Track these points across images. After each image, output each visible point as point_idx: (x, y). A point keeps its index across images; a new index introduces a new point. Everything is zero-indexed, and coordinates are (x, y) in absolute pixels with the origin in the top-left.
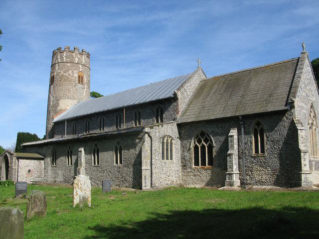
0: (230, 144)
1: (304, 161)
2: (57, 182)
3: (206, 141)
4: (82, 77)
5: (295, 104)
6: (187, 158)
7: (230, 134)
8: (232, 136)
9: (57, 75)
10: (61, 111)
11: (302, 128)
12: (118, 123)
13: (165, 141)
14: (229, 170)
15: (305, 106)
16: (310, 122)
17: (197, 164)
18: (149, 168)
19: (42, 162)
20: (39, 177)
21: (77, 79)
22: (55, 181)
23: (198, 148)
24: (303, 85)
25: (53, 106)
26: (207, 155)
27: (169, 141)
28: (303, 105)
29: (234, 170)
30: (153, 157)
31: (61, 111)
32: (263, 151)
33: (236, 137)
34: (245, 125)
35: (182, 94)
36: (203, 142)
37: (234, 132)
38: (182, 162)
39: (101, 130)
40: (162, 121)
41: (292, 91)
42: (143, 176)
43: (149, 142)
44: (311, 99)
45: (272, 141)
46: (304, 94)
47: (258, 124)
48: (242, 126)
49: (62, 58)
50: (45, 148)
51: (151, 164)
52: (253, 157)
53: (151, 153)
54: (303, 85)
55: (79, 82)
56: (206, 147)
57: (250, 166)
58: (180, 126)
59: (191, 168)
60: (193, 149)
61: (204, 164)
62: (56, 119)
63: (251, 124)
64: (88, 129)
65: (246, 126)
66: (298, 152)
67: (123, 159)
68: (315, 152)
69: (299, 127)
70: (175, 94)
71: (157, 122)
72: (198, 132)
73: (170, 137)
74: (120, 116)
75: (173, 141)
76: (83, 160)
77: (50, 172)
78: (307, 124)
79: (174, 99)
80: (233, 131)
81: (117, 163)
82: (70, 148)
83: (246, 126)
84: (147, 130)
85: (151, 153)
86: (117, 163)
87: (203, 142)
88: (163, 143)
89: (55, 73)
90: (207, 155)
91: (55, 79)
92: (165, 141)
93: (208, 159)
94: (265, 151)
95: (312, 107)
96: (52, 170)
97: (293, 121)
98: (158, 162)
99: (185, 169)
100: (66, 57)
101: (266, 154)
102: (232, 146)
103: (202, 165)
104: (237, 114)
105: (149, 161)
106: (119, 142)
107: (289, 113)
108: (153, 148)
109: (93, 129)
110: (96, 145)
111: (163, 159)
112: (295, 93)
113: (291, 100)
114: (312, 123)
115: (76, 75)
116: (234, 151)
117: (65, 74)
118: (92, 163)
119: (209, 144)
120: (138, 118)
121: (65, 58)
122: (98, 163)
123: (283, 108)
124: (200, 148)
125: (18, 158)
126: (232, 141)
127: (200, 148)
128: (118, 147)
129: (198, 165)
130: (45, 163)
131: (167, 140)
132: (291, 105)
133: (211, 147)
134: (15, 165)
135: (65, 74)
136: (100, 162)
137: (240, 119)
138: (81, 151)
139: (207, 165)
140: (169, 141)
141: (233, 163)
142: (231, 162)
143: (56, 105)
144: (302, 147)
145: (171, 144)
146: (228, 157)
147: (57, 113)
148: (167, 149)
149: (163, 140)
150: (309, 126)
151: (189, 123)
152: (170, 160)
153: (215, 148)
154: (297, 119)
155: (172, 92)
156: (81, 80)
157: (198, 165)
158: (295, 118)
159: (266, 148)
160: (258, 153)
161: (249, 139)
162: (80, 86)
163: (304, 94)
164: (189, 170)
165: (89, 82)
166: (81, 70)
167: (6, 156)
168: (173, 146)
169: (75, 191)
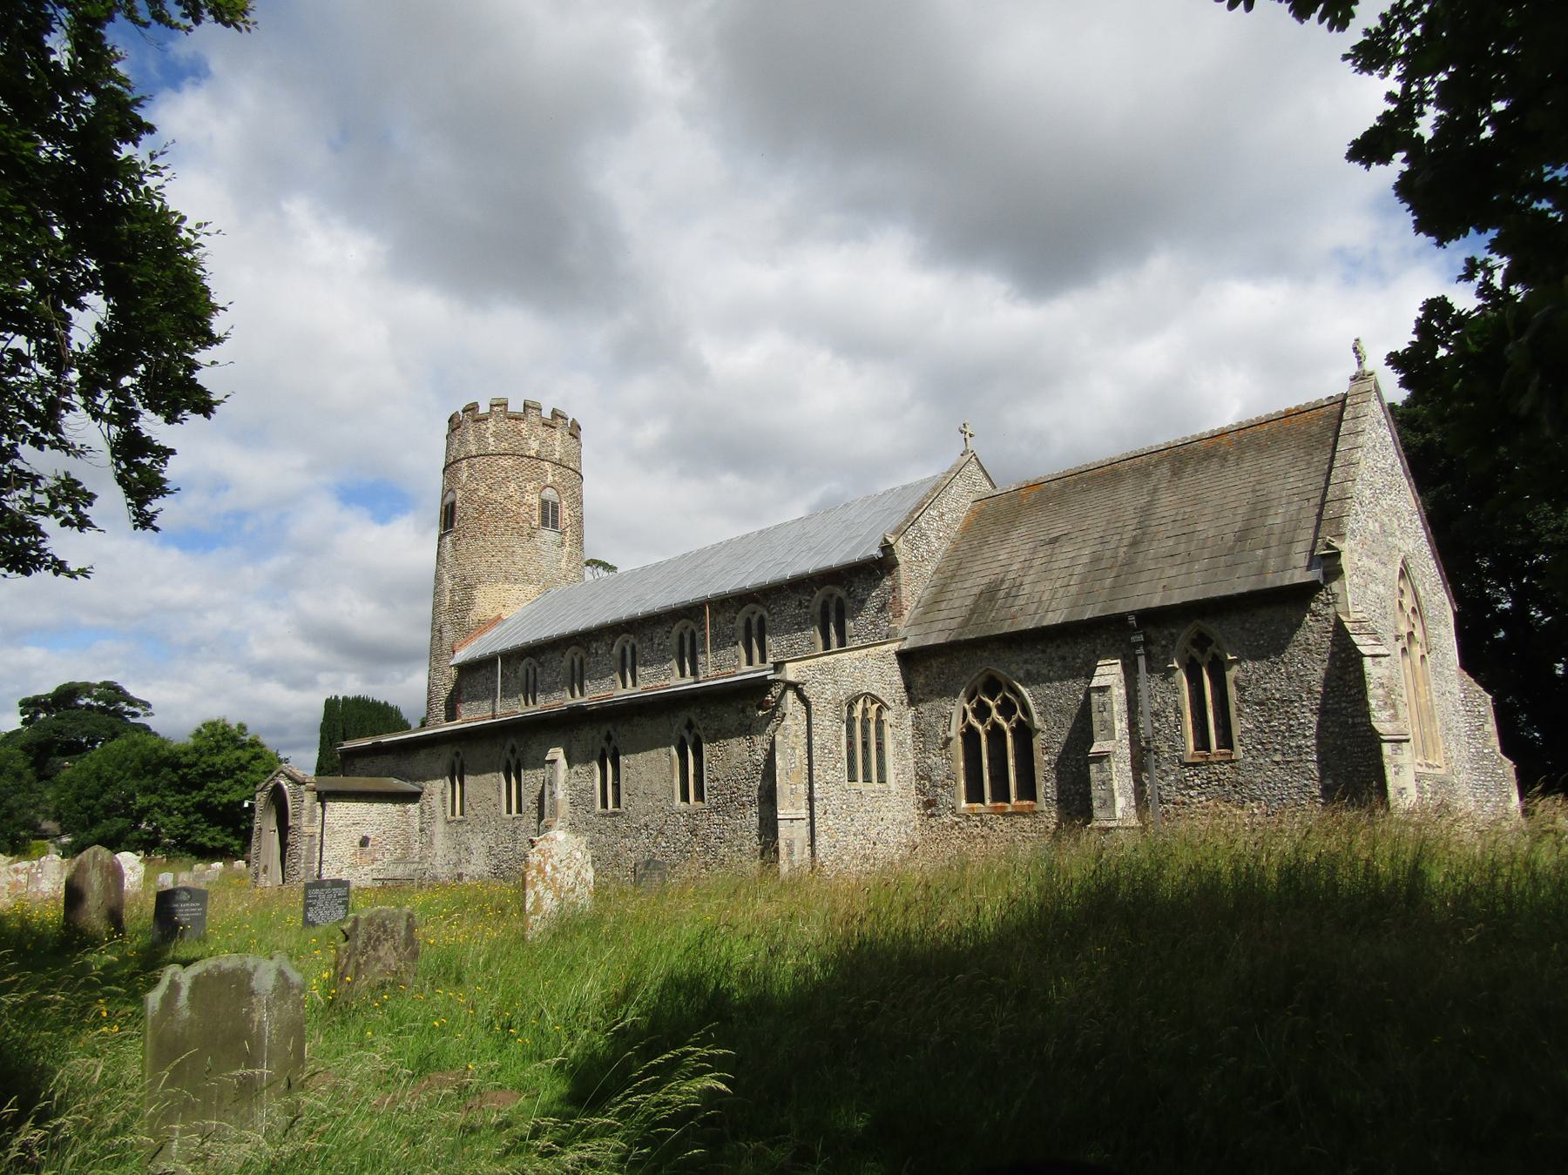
0: (1096, 718)
1: (1397, 773)
2: (466, 879)
3: (1007, 709)
4: (555, 507)
5: (1345, 562)
6: (938, 776)
7: (1095, 683)
8: (1103, 689)
9: (467, 500)
10: (486, 625)
11: (1379, 650)
12: (688, 654)
13: (858, 713)
14: (1097, 813)
15: (1381, 572)
16: (1404, 629)
17: (975, 794)
18: (804, 813)
19: (413, 808)
20: (398, 861)
21: (536, 514)
22: (460, 876)
23: (1004, 734)
24: (1368, 493)
25: (453, 608)
26: (1011, 762)
27: (872, 714)
28: (1372, 564)
29: (1119, 814)
30: (815, 773)
31: (486, 625)
32: (1226, 740)
33: (1119, 692)
34: (1150, 647)
35: (914, 547)
36: (994, 712)
37: (1109, 673)
38: (921, 791)
39: (573, 695)
40: (842, 643)
41: (1329, 512)
42: (782, 844)
43: (802, 717)
44: (1400, 544)
45: (1261, 704)
46: (1373, 526)
47: (1202, 641)
48: (1141, 651)
49: (480, 438)
50: (423, 754)
51: (811, 799)
52: (1187, 765)
53: (810, 758)
54: (1368, 493)
55: (544, 523)
56: (1009, 734)
57: (1179, 798)
58: (907, 659)
59: (953, 810)
60: (958, 745)
61: (1001, 794)
62: (462, 655)
63: (1174, 642)
64: (576, 679)
65: (1155, 649)
66: (1373, 741)
67: (706, 784)
68: (1429, 743)
69: (1364, 644)
70: (887, 548)
71: (827, 646)
72: (976, 675)
73: (875, 699)
74: (693, 634)
75: (886, 715)
76: (562, 794)
77: (441, 845)
78: (1390, 637)
79: (881, 566)
80: (1106, 670)
81: (685, 798)
82: (513, 751)
83: (1155, 649)
84: (791, 672)
85: (810, 758)
86: (685, 798)
87: (994, 712)
88: (850, 722)
89: (459, 493)
90: (1011, 762)
91: (459, 514)
92: (858, 713)
93: (1018, 776)
94: (1235, 740)
95: (1403, 574)
96: (449, 836)
97: (1339, 624)
98: (835, 791)
99: (932, 815)
100: (495, 435)
101: (1239, 752)
102: (1109, 729)
103: (994, 799)
104: (1121, 607)
105: (803, 788)
106: (690, 721)
107: (1322, 596)
108: (816, 740)
109: (548, 690)
110: (609, 738)
111: (852, 779)
112: (1338, 520)
113: (1329, 547)
114: (1411, 634)
115: (535, 500)
116: (1114, 742)
117: (493, 496)
118: (592, 801)
119: (1019, 721)
120: (755, 636)
121: (491, 440)
122: (617, 803)
123: (1300, 576)
124: (983, 737)
125: (324, 797)
126: (1104, 707)
127: (983, 737)
128: (513, 763)
129: (982, 801)
130: (422, 812)
131: (865, 711)
132: (1330, 565)
133: (1025, 733)
134: (312, 820)
135: (493, 496)
136: (624, 798)
137: (1130, 627)
138: (553, 761)
139: (1013, 799)
140: (872, 714)
141: (1112, 790)
142: (1107, 782)
143: (463, 605)
144: (1381, 721)
145: (880, 723)
146: (1093, 768)
147: (467, 633)
148: (865, 745)
149: (851, 707)
150: (1399, 645)
151: (1241, 596)
152: (875, 785)
153: (1041, 736)
154: (1354, 616)
155: (878, 541)
156: (549, 514)
157: (982, 801)
158: (1348, 614)
159: (1236, 731)
160: (1207, 747)
161: (1171, 699)
162: (548, 535)
163: (1373, 526)
164: (948, 819)
165: (580, 521)
166: (550, 479)
167: (278, 788)
168: (888, 731)
169: (530, 894)
